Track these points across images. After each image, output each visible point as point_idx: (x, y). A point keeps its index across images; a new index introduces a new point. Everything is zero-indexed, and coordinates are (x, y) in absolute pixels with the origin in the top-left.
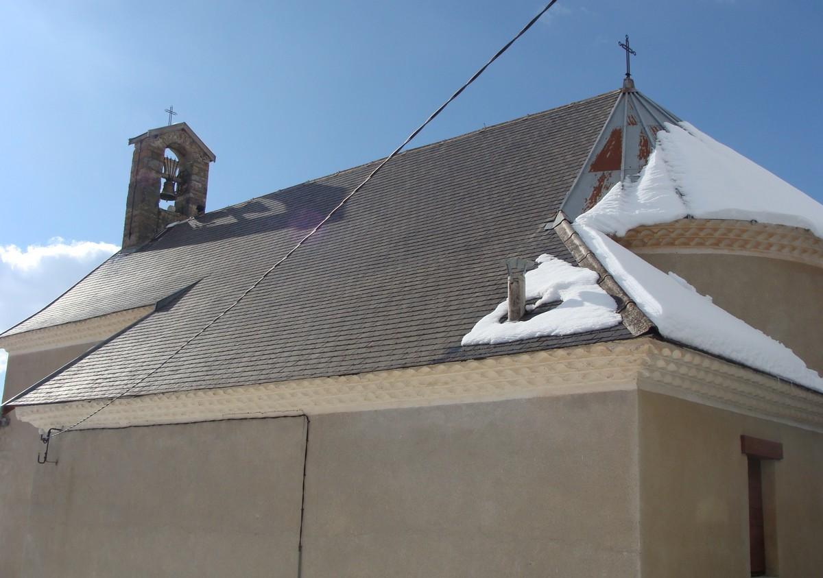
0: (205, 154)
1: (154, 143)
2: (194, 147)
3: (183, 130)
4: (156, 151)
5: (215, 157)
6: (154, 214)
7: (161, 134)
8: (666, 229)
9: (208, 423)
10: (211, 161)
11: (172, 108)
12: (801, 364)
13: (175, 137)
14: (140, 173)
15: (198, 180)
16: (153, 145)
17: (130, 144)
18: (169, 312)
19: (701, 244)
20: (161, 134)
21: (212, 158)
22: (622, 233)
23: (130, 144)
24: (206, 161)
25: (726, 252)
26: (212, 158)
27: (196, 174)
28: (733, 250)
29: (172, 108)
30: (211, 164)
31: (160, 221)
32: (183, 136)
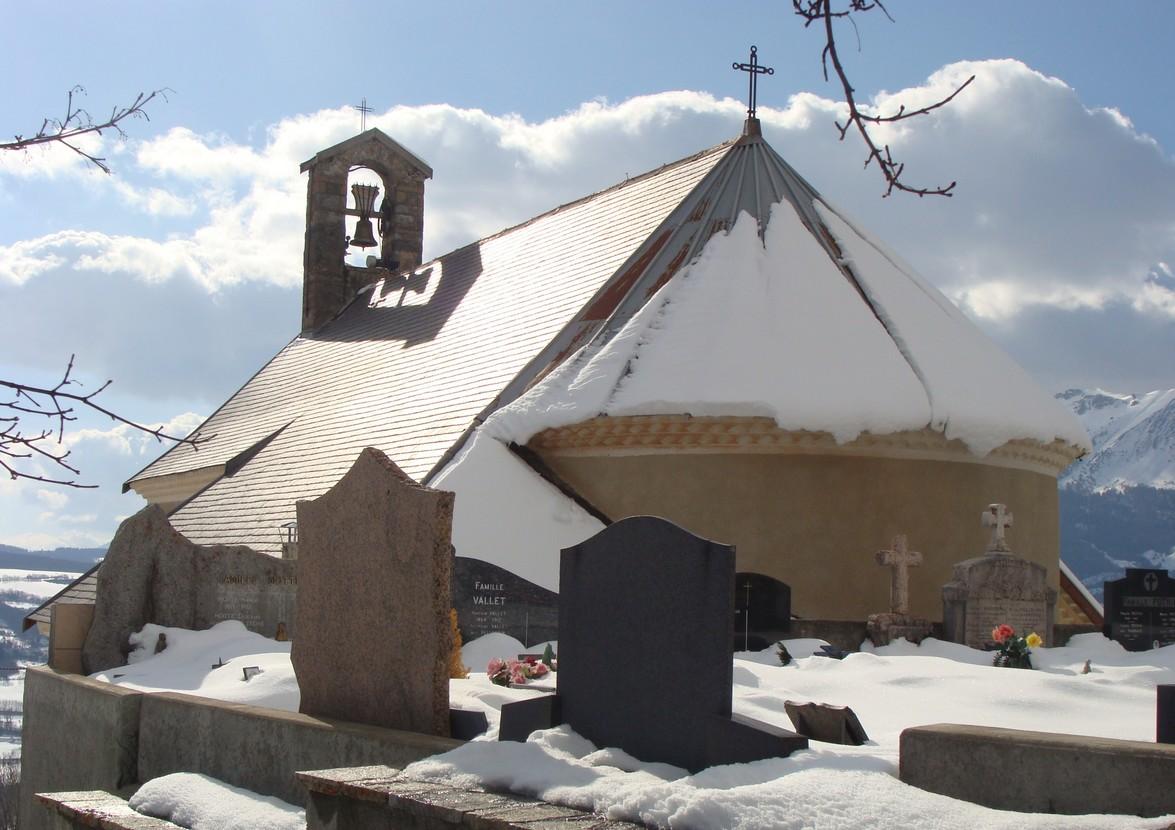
0: (416, 169)
1: (328, 170)
2: (395, 161)
3: (375, 139)
4: (332, 181)
5: (431, 170)
6: (339, 276)
7: (339, 154)
8: (587, 428)
9: (890, 13)
10: (426, 178)
11: (364, 102)
12: (817, 98)
13: (363, 153)
14: (314, 218)
15: (407, 212)
16: (326, 173)
17: (302, 171)
18: (232, 480)
19: (637, 443)
20: (339, 154)
21: (428, 173)
22: (522, 441)
23: (302, 171)
24: (418, 179)
25: (672, 451)
26: (428, 173)
27: (403, 203)
28: (682, 448)
29: (364, 102)
30: (427, 183)
31: (349, 285)
32: (376, 148)
